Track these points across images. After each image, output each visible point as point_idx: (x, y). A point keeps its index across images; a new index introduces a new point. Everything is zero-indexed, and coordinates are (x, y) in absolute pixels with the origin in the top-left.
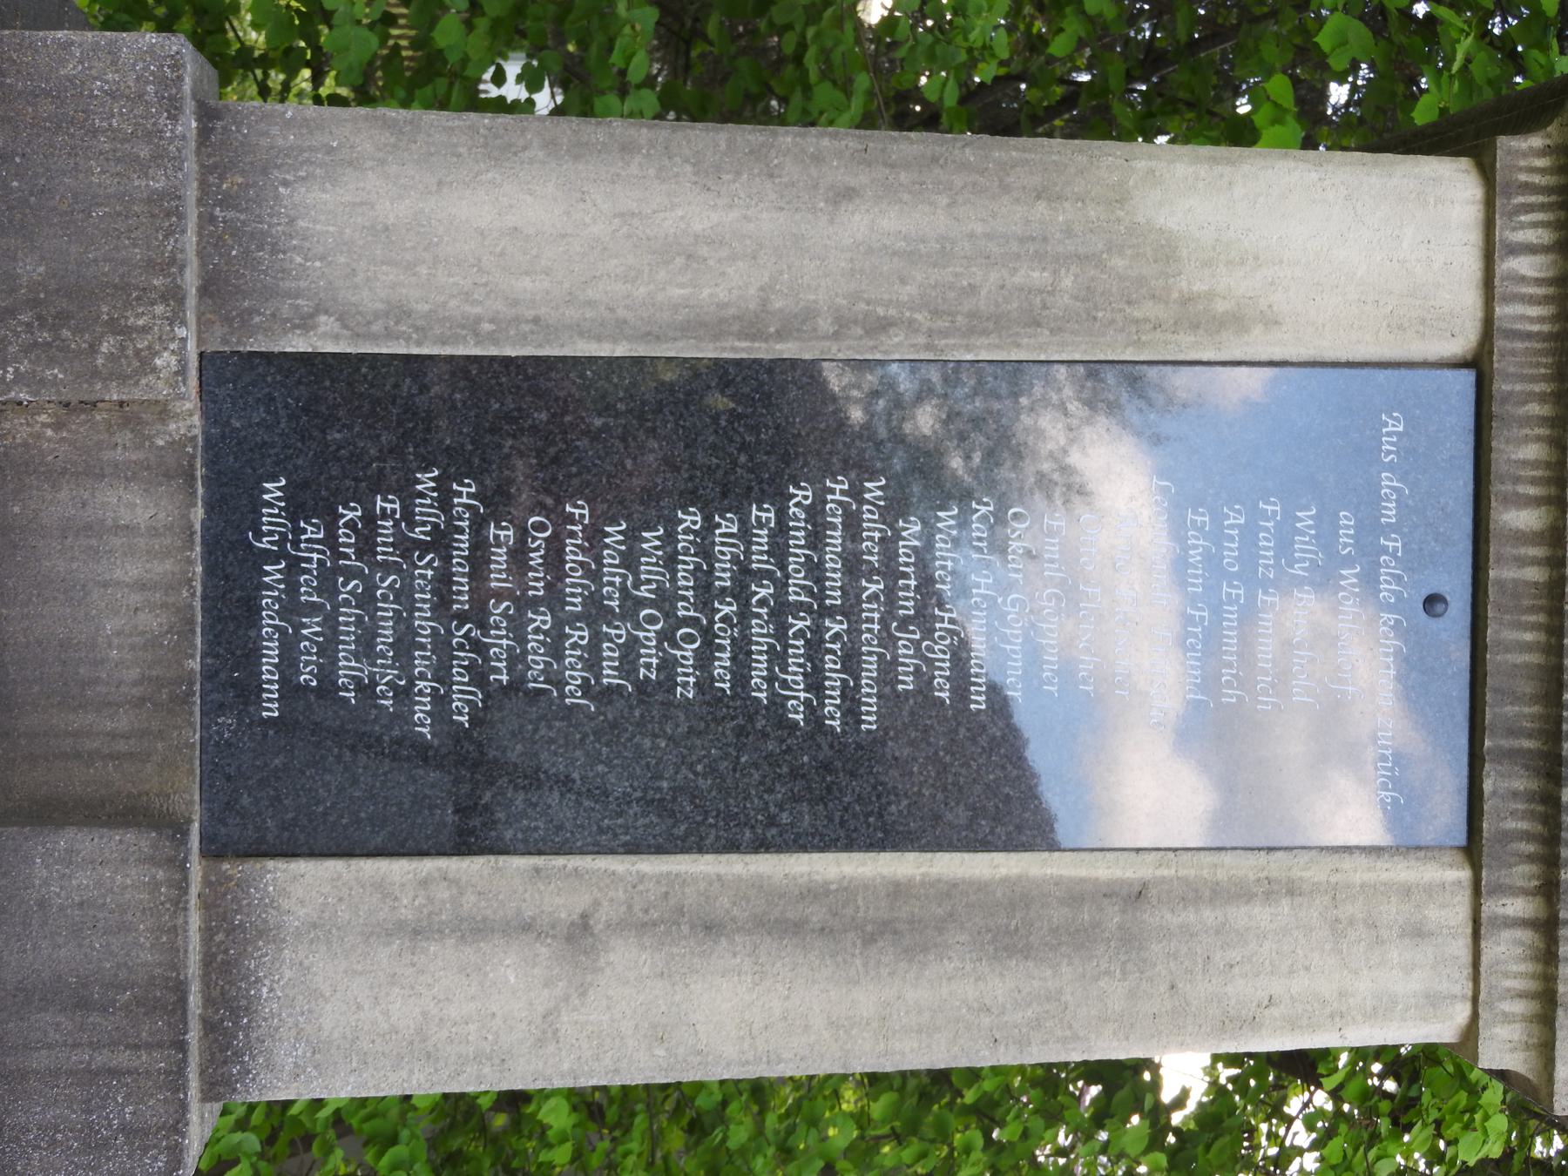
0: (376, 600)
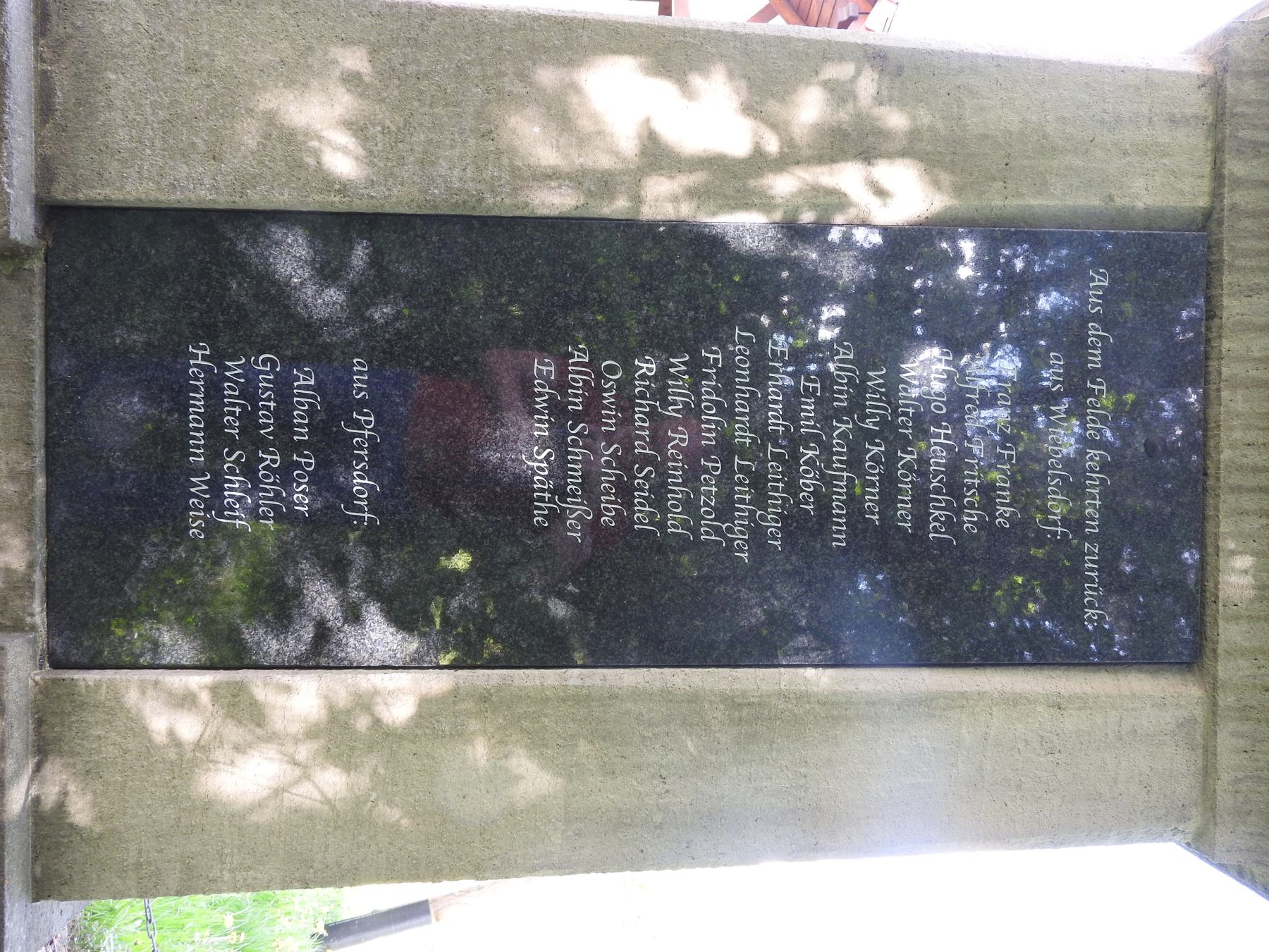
0: (567, 445)
